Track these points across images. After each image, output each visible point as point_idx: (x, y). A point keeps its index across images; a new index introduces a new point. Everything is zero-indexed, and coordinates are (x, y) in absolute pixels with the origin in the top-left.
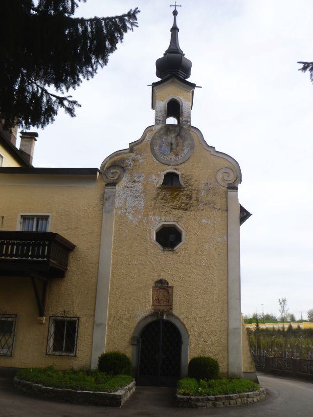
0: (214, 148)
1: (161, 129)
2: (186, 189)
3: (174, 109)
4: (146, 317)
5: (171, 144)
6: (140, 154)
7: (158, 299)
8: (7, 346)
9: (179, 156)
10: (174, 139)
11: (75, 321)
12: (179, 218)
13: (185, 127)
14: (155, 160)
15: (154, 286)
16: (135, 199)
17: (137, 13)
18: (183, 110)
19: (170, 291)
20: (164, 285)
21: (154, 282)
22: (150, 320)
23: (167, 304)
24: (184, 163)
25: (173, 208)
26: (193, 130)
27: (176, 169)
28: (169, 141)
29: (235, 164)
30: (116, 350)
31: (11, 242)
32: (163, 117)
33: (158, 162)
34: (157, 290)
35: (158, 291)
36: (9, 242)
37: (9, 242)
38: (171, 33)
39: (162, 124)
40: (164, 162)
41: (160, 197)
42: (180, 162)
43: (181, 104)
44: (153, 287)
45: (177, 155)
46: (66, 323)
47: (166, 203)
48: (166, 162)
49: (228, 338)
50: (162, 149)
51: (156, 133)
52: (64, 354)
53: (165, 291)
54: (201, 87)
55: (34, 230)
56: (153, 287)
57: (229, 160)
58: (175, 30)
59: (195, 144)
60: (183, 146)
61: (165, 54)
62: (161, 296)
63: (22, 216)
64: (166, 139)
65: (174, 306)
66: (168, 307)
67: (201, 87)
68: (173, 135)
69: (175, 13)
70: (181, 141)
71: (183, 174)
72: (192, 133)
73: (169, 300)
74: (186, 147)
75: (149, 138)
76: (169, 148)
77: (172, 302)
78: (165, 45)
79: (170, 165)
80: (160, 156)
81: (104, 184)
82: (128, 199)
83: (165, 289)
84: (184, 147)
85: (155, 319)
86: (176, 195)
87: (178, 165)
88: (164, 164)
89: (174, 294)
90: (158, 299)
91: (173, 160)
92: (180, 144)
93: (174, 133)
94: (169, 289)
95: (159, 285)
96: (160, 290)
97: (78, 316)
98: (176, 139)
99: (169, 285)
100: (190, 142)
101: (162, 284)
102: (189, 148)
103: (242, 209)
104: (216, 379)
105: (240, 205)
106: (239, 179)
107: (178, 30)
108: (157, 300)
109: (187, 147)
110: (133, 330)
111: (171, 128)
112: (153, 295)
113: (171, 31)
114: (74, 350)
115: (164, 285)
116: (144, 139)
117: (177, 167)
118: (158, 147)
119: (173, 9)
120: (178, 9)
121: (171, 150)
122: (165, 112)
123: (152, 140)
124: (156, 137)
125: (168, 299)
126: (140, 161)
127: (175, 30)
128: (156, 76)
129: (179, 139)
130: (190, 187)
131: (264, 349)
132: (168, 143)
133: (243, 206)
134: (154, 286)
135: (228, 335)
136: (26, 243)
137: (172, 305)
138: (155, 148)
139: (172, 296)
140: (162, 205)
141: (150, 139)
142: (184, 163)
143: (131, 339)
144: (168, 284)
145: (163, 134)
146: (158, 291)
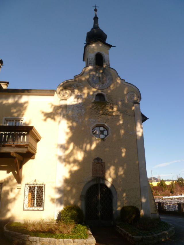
0: (124, 80)
2: (109, 103)
3: (99, 60)
4: (89, 182)
6: (81, 83)
9: (104, 84)
11: (43, 186)
12: (106, 120)
16: (79, 109)
18: (105, 59)
22: (92, 184)
25: (102, 115)
26: (111, 70)
29: (137, 90)
31: (22, 133)
32: (94, 62)
36: (6, 133)
37: (25, 133)
38: (93, 20)
41: (94, 108)
43: (103, 56)
45: (103, 83)
46: (36, 188)
47: (98, 111)
49: (141, 193)
52: (36, 209)
54: (115, 47)
55: (20, 125)
58: (96, 19)
61: (91, 30)
63: (5, 119)
67: (115, 47)
69: (96, 10)
70: (105, 76)
71: (107, 95)
73: (103, 171)
78: (92, 26)
81: (60, 99)
82: (74, 109)
85: (95, 183)
86: (104, 106)
87: (103, 89)
90: (96, 170)
97: (44, 183)
98: (102, 75)
103: (143, 116)
105: (142, 113)
106: (140, 98)
107: (98, 18)
108: (95, 171)
109: (109, 80)
110: (81, 191)
113: (94, 19)
114: (42, 206)
117: (103, 90)
118: (91, 79)
119: (95, 8)
120: (97, 8)
121: (100, 81)
122: (94, 59)
126: (81, 86)
127: (96, 19)
130: (112, 102)
133: (143, 113)
135: (140, 191)
136: (4, 133)
140: (96, 112)
143: (81, 197)
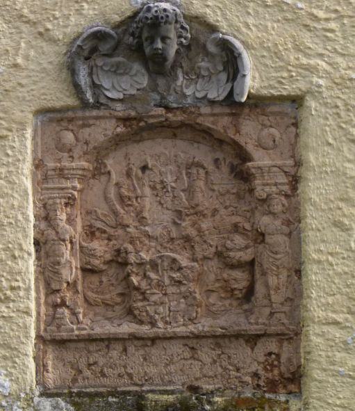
7: (119, 260)
8: (282, 181)
15: (61, 97)
17: (195, 335)
19: (261, 160)
20: (188, 89)
21: (52, 56)
23: (232, 319)
30: (251, 152)
34: (99, 155)
35: (114, 164)
44: (50, 116)
53: (202, 154)
56: (50, 116)
62: (158, 217)
65: (316, 339)
66: (249, 360)
77: (296, 297)
83: (205, 135)
89: (315, 190)
90: (119, 260)
94: (249, 132)
95: (114, 88)
96: (142, 152)
99: (252, 82)
101: (157, 65)
104: (148, 164)
112: (46, 216)
115: (188, 89)
125: (240, 249)
134: (61, 97)
137: (293, 334)
139: (294, 223)
144: (231, 62)
146: (114, 164)
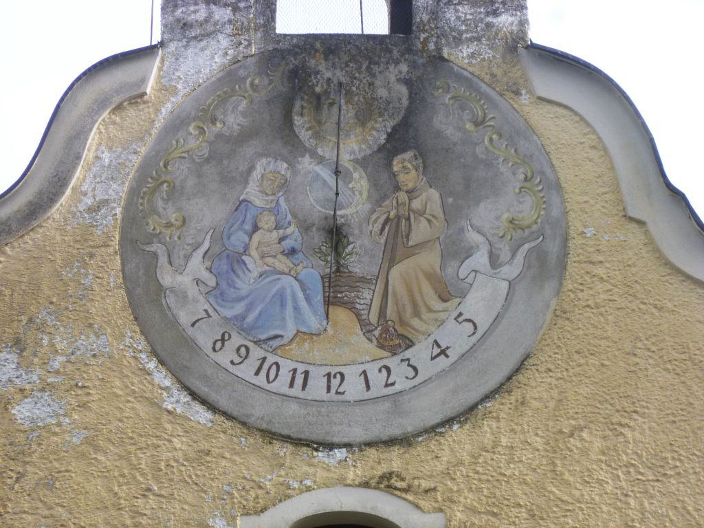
1: (230, 78)
5: (336, 235)
9: (420, 353)
10: (360, 182)
13: (461, 55)
14: (177, 401)
24: (466, 414)
26: (546, 83)
27: (386, 483)
28: (314, 203)
33: (202, 415)
39: (240, 30)
40: (259, 410)
42: (426, 409)
48: (291, 417)
50: (245, 283)
51: (176, 125)
57: (567, 60)
59: (575, 225)
60: (457, 251)
64: (284, 185)
68: (354, 146)
70: (431, 198)
72: (540, 118)
74: (480, 259)
75: (116, 170)
76: (313, 271)
79: (330, 446)
80: (225, 357)
84: (468, 253)
87: (404, 441)
88: (270, 435)
91: (353, 388)
92: (420, 231)
93: (363, 118)
100: (527, 210)
102: (511, 270)
109: (494, 261)
111: (326, 72)
116: (71, 158)
117: (395, 460)
118: (196, 265)
123: (134, 192)
124: (180, 171)
128: (391, 369)
129: (409, 179)
131: (539, 467)
132: (305, 227)
138: (167, 278)
141: (119, 191)
142: (466, 414)
145: (244, 137)
